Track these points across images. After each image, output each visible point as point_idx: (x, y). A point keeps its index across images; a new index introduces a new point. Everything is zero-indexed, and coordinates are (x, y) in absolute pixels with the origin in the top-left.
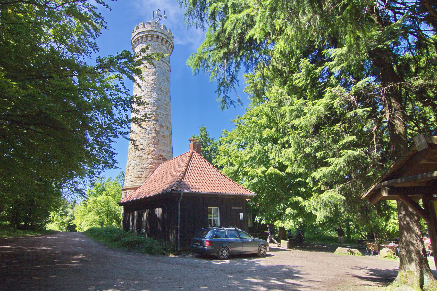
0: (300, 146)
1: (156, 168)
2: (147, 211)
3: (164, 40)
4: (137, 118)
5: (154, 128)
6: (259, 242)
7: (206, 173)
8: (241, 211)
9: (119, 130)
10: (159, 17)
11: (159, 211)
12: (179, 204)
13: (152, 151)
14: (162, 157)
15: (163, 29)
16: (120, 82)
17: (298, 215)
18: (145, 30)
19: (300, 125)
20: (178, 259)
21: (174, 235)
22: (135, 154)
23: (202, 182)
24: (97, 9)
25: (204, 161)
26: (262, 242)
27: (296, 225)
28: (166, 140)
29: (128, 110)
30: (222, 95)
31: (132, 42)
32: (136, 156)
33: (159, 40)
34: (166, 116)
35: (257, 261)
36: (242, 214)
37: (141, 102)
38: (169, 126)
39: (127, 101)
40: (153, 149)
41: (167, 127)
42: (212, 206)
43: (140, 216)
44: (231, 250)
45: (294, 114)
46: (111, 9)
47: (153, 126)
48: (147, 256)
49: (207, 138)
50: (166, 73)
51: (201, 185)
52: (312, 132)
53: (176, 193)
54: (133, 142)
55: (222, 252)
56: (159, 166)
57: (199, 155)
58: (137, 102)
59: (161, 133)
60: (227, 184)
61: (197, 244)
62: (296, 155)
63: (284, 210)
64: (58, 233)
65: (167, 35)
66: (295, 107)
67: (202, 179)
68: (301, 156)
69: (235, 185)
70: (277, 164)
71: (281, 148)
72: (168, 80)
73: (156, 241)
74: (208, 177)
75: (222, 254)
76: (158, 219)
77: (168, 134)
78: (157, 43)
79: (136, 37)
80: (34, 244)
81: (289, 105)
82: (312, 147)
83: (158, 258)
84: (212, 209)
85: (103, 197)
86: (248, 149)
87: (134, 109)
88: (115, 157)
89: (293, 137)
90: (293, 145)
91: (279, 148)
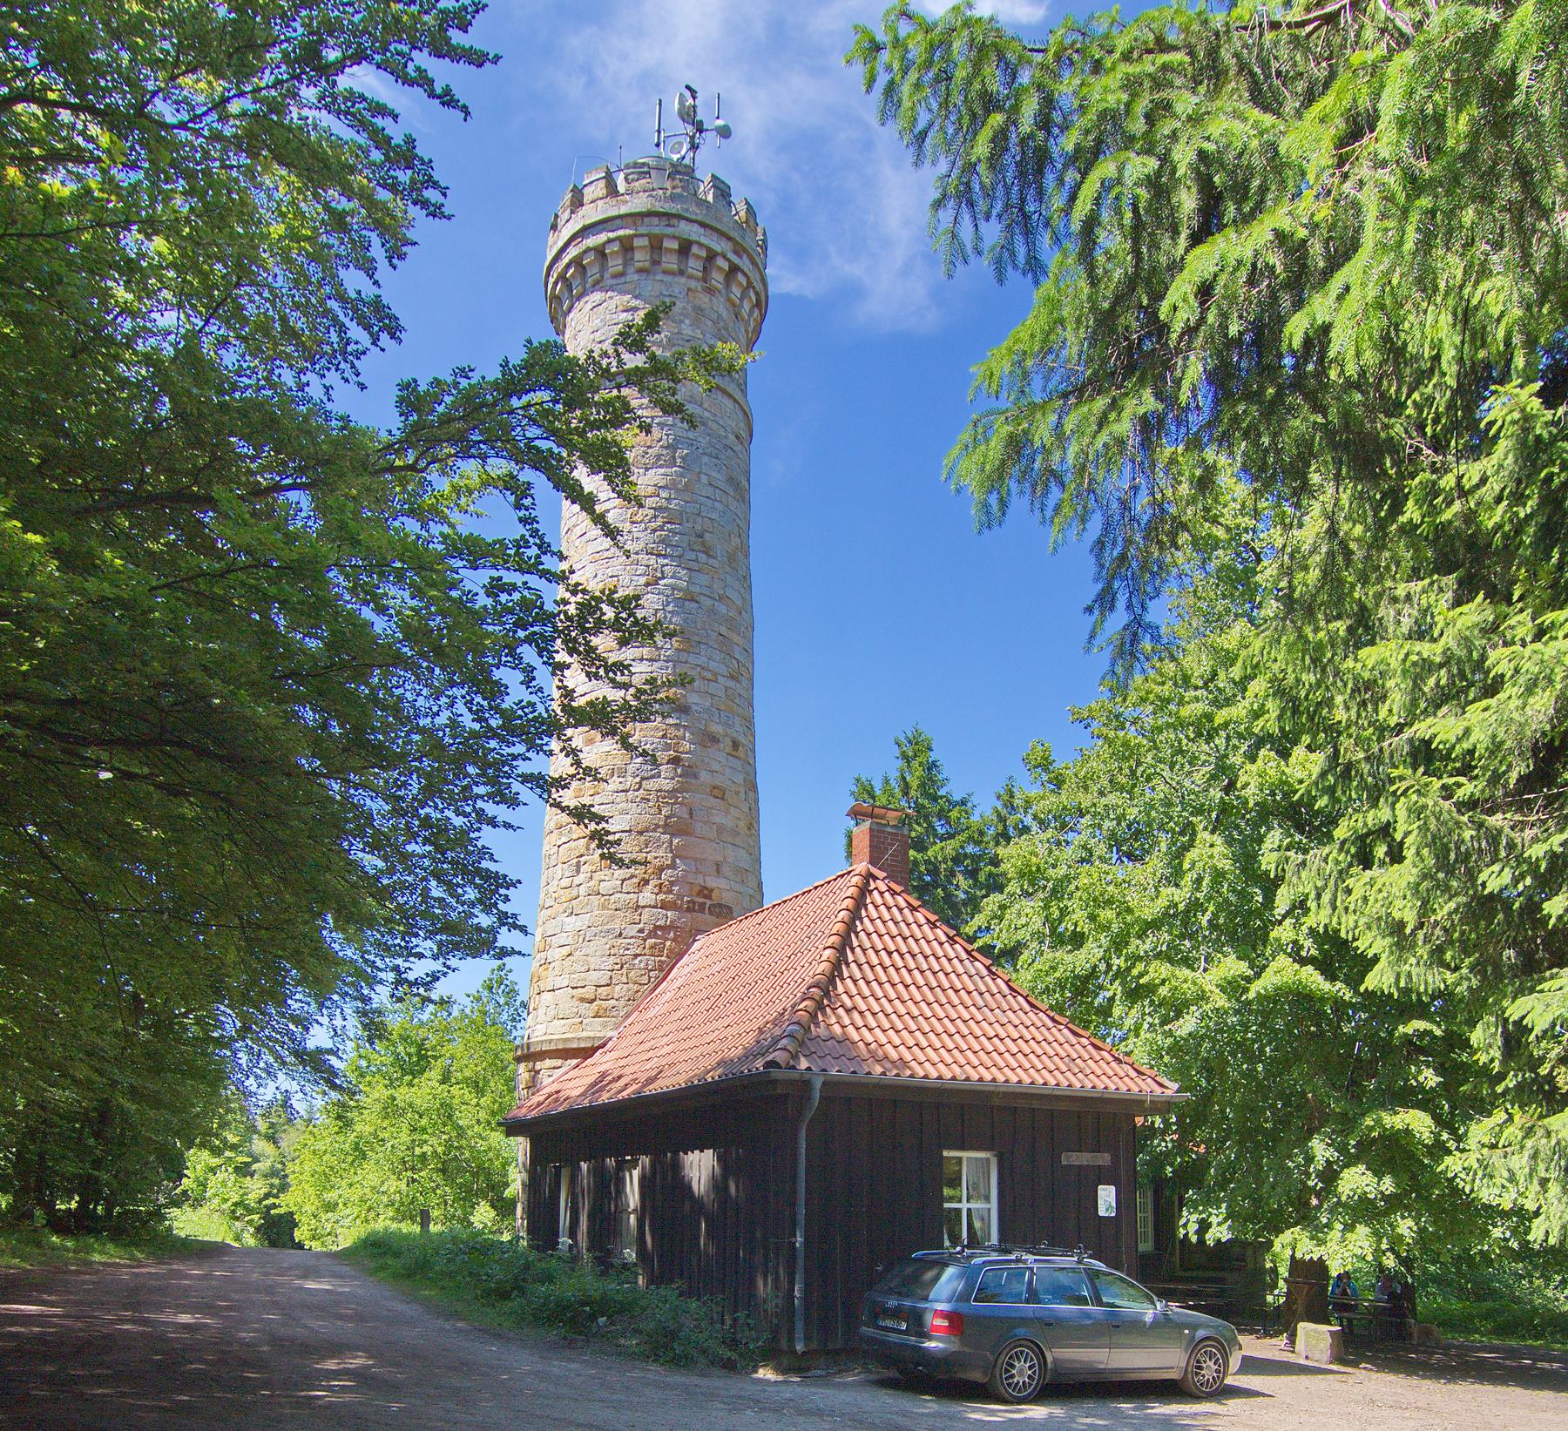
0: (1452, 856)
1: (681, 956)
2: (645, 1160)
3: (720, 262)
4: (609, 704)
5: (667, 747)
6: (1194, 1327)
7: (934, 984)
8: (1104, 1177)
9: (523, 767)
10: (690, 129)
11: (700, 1167)
12: (803, 1134)
13: (661, 869)
14: (709, 897)
15: (710, 198)
16: (522, 513)
17: (1394, 1203)
18: (614, 213)
19: (1466, 745)
20: (799, 1390)
21: (776, 1280)
22: (577, 880)
23: (914, 1027)
24: (395, 117)
25: (922, 920)
26: (1208, 1326)
27: (1384, 1253)
28: (727, 812)
29: (568, 666)
30: (1119, 618)
31: (551, 280)
32: (583, 891)
33: (692, 263)
34: (731, 684)
35: (1182, 1415)
36: (1113, 1188)
37: (636, 623)
38: (742, 739)
39: (569, 619)
40: (660, 855)
41: (736, 745)
42: (963, 1148)
43: (607, 1187)
44: (1055, 1360)
45: (1431, 682)
46: (465, 110)
47: (664, 736)
48: (654, 1371)
49: (934, 799)
50: (727, 447)
51: (911, 1042)
52: (1521, 779)
53: (793, 1082)
54: (593, 826)
55: (1013, 1366)
56: (696, 945)
57: (898, 889)
58: (616, 625)
59: (704, 776)
60: (1040, 1038)
61: (889, 1323)
62: (1425, 903)
63: (1330, 1175)
64: (226, 1254)
65: (733, 234)
66: (1438, 648)
67: (916, 1012)
68: (1452, 905)
69: (1080, 1048)
70: (1308, 943)
71: (1350, 865)
72: (739, 487)
73: (693, 1303)
74: (944, 1001)
75: (1013, 1376)
76: (697, 1203)
77: (739, 778)
78: (683, 280)
79: (573, 252)
80: (137, 1297)
81: (1405, 630)
82: (1520, 860)
83: (705, 1382)
84: (960, 1159)
85: (424, 1091)
86: (1156, 863)
87: (605, 660)
88: (507, 899)
89: (1417, 812)
90: (1413, 850)
91: (1337, 863)
